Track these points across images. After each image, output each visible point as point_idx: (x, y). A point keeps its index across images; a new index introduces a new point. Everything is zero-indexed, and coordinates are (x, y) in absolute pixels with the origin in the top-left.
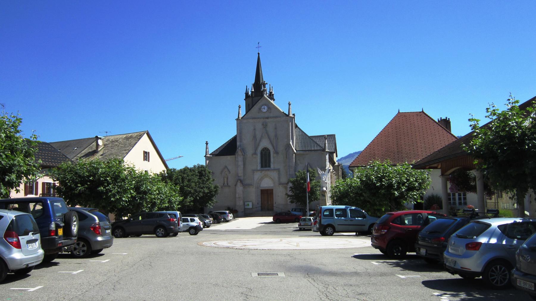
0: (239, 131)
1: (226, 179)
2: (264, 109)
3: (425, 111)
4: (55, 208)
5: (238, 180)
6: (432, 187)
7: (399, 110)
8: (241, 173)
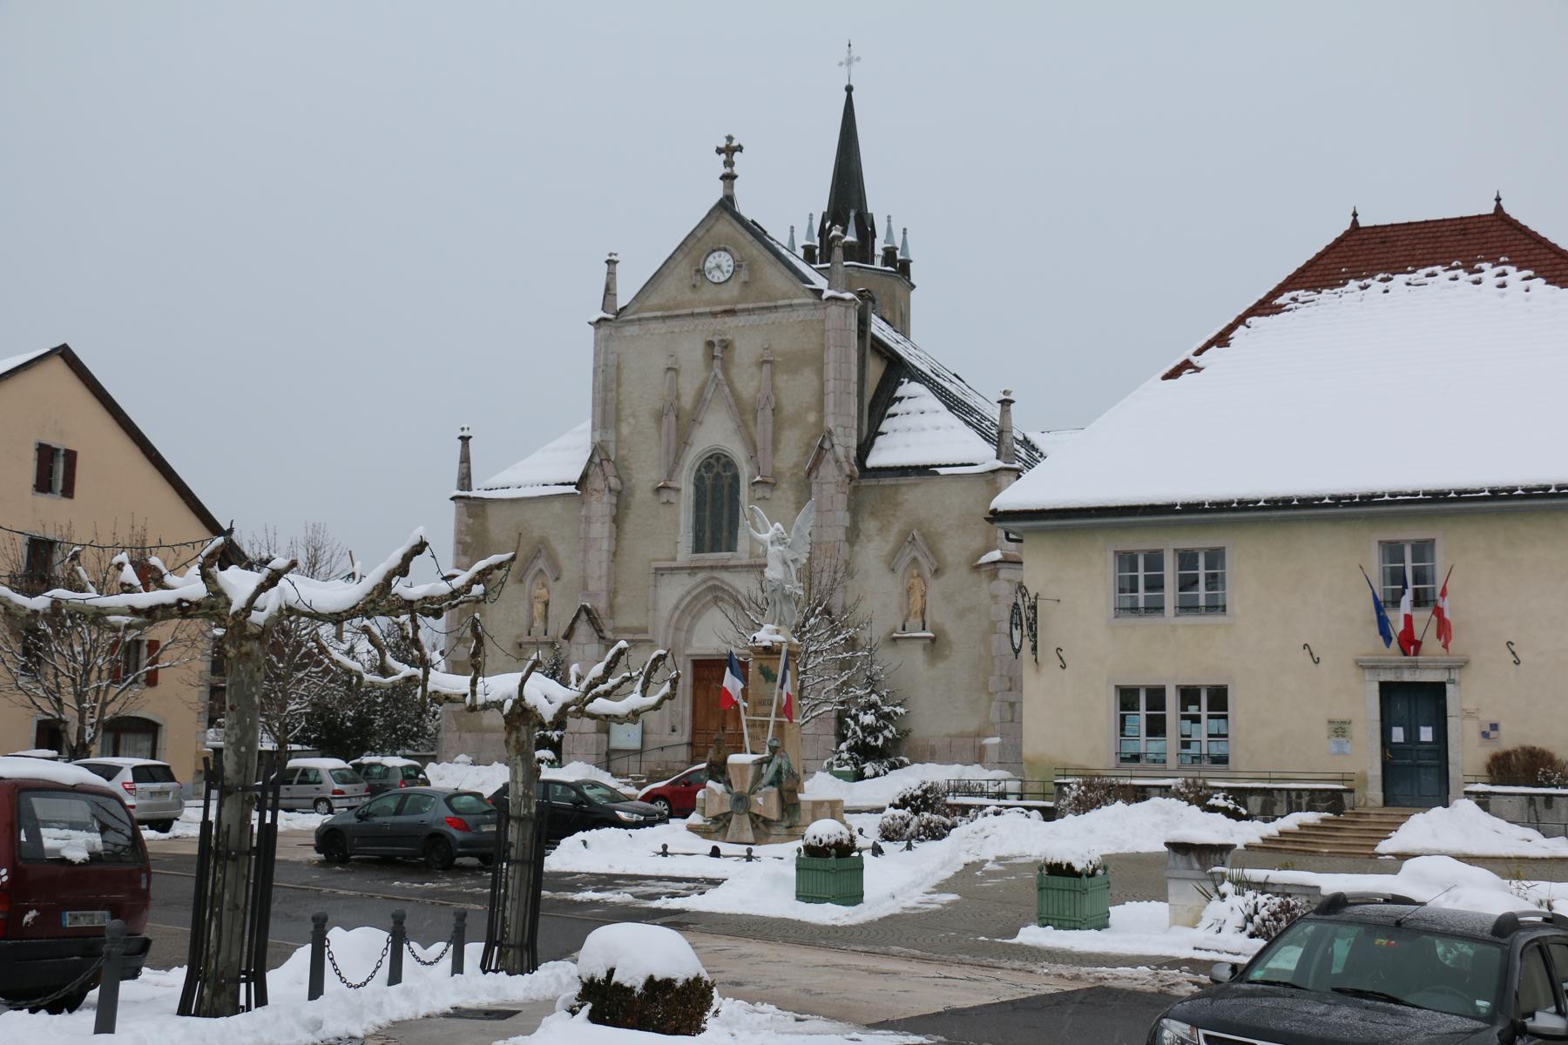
0: (601, 378)
1: (539, 608)
2: (718, 267)
3: (1512, 210)
4: (520, 858)
5: (580, 611)
6: (1509, 643)
7: (1355, 215)
8: (598, 585)
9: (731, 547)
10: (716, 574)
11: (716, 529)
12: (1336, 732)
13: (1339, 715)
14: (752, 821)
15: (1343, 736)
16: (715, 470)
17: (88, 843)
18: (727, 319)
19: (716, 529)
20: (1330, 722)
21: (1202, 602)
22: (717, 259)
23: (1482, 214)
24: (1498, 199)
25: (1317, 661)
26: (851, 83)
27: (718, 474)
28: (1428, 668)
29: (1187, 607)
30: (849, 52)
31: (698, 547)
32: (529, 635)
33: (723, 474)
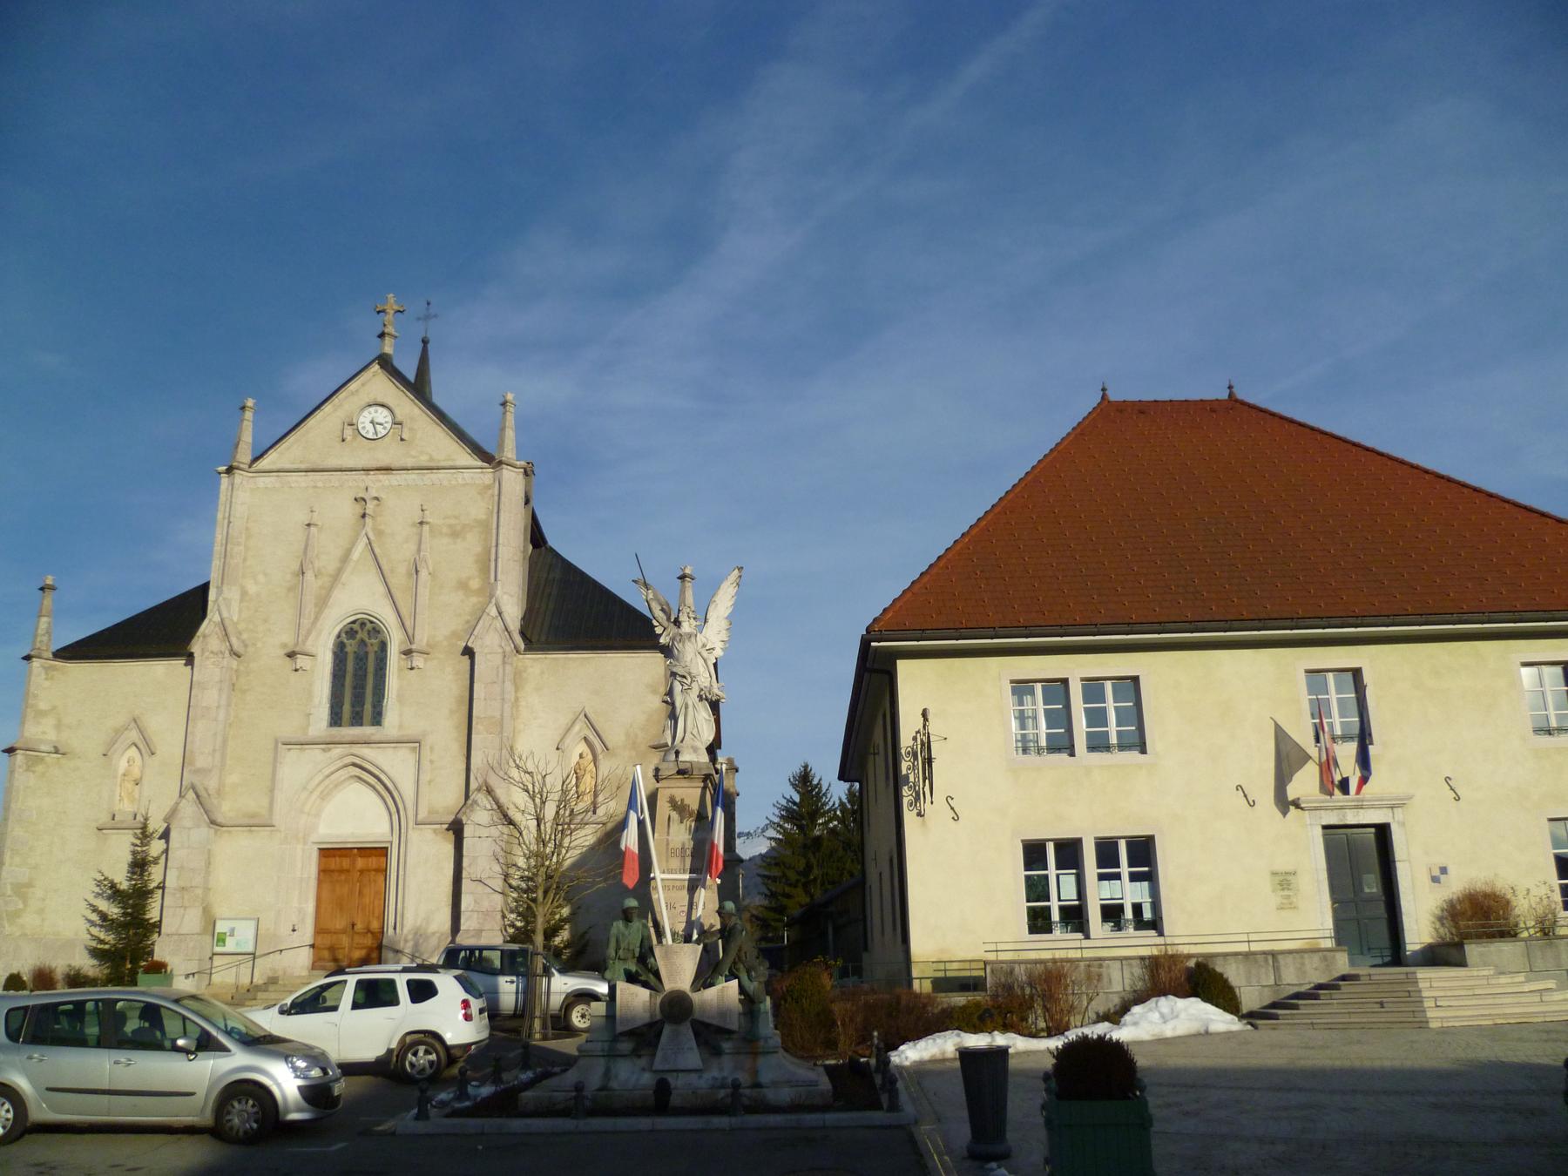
6: (1447, 779)
9: (377, 719)
10: (357, 749)
11: (358, 699)
12: (1281, 885)
13: (1282, 865)
14: (697, 1035)
15: (1289, 889)
16: (359, 636)
17: (142, 974)
18: (381, 477)
19: (358, 699)
20: (1274, 874)
21: (1114, 740)
22: (374, 415)
23: (1204, 399)
24: (1230, 387)
25: (1252, 804)
26: (428, 336)
27: (362, 641)
28: (1372, 807)
29: (1098, 744)
30: (428, 309)
31: (336, 719)
32: (113, 819)
33: (367, 640)
